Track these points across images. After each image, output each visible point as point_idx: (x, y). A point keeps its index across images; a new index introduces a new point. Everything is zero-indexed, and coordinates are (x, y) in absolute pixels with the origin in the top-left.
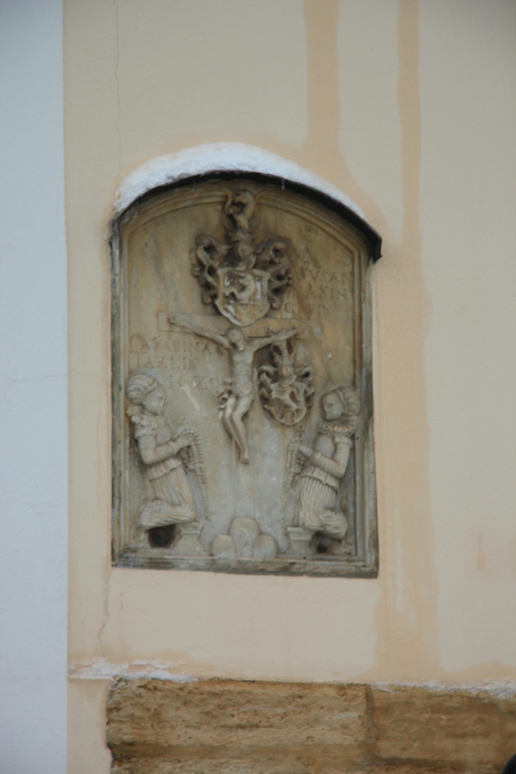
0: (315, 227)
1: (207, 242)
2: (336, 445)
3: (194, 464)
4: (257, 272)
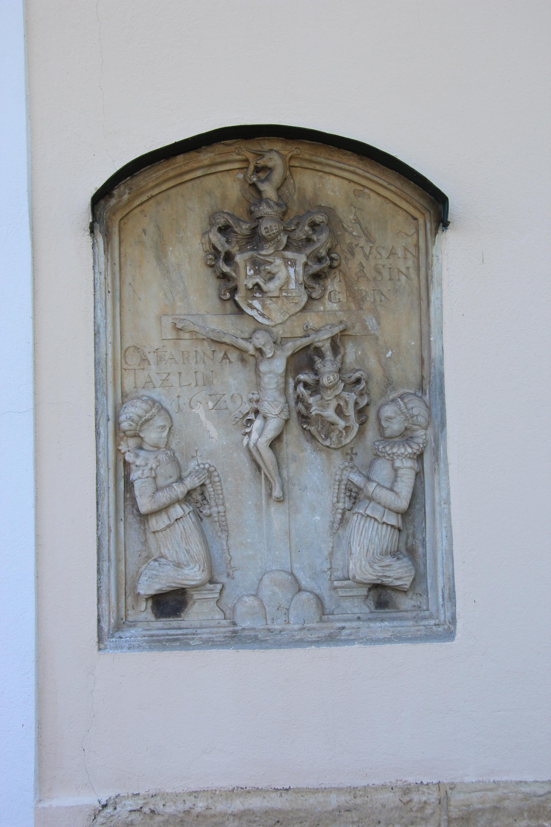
0: (366, 191)
1: (221, 221)
2: (396, 470)
3: (210, 508)
4: (289, 254)
